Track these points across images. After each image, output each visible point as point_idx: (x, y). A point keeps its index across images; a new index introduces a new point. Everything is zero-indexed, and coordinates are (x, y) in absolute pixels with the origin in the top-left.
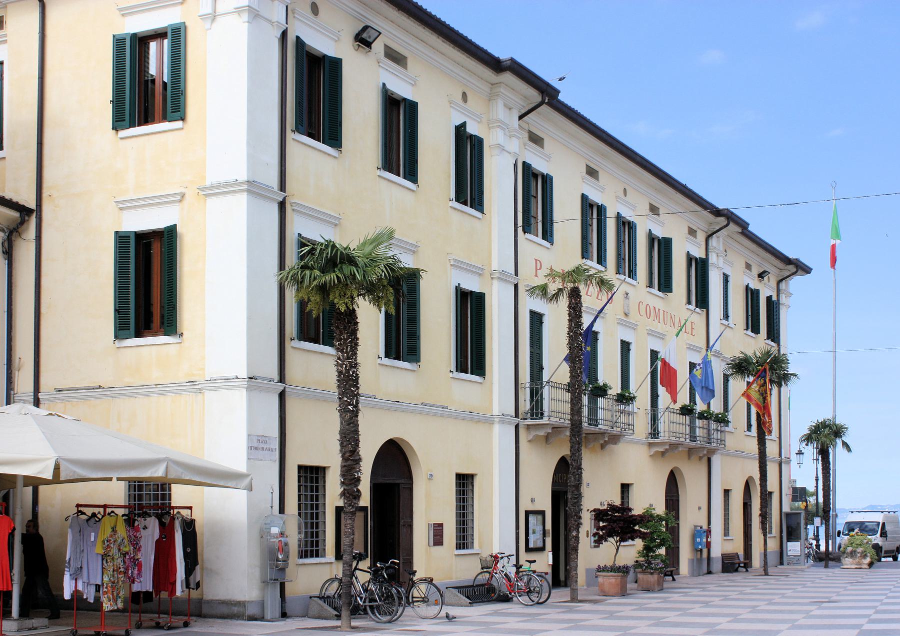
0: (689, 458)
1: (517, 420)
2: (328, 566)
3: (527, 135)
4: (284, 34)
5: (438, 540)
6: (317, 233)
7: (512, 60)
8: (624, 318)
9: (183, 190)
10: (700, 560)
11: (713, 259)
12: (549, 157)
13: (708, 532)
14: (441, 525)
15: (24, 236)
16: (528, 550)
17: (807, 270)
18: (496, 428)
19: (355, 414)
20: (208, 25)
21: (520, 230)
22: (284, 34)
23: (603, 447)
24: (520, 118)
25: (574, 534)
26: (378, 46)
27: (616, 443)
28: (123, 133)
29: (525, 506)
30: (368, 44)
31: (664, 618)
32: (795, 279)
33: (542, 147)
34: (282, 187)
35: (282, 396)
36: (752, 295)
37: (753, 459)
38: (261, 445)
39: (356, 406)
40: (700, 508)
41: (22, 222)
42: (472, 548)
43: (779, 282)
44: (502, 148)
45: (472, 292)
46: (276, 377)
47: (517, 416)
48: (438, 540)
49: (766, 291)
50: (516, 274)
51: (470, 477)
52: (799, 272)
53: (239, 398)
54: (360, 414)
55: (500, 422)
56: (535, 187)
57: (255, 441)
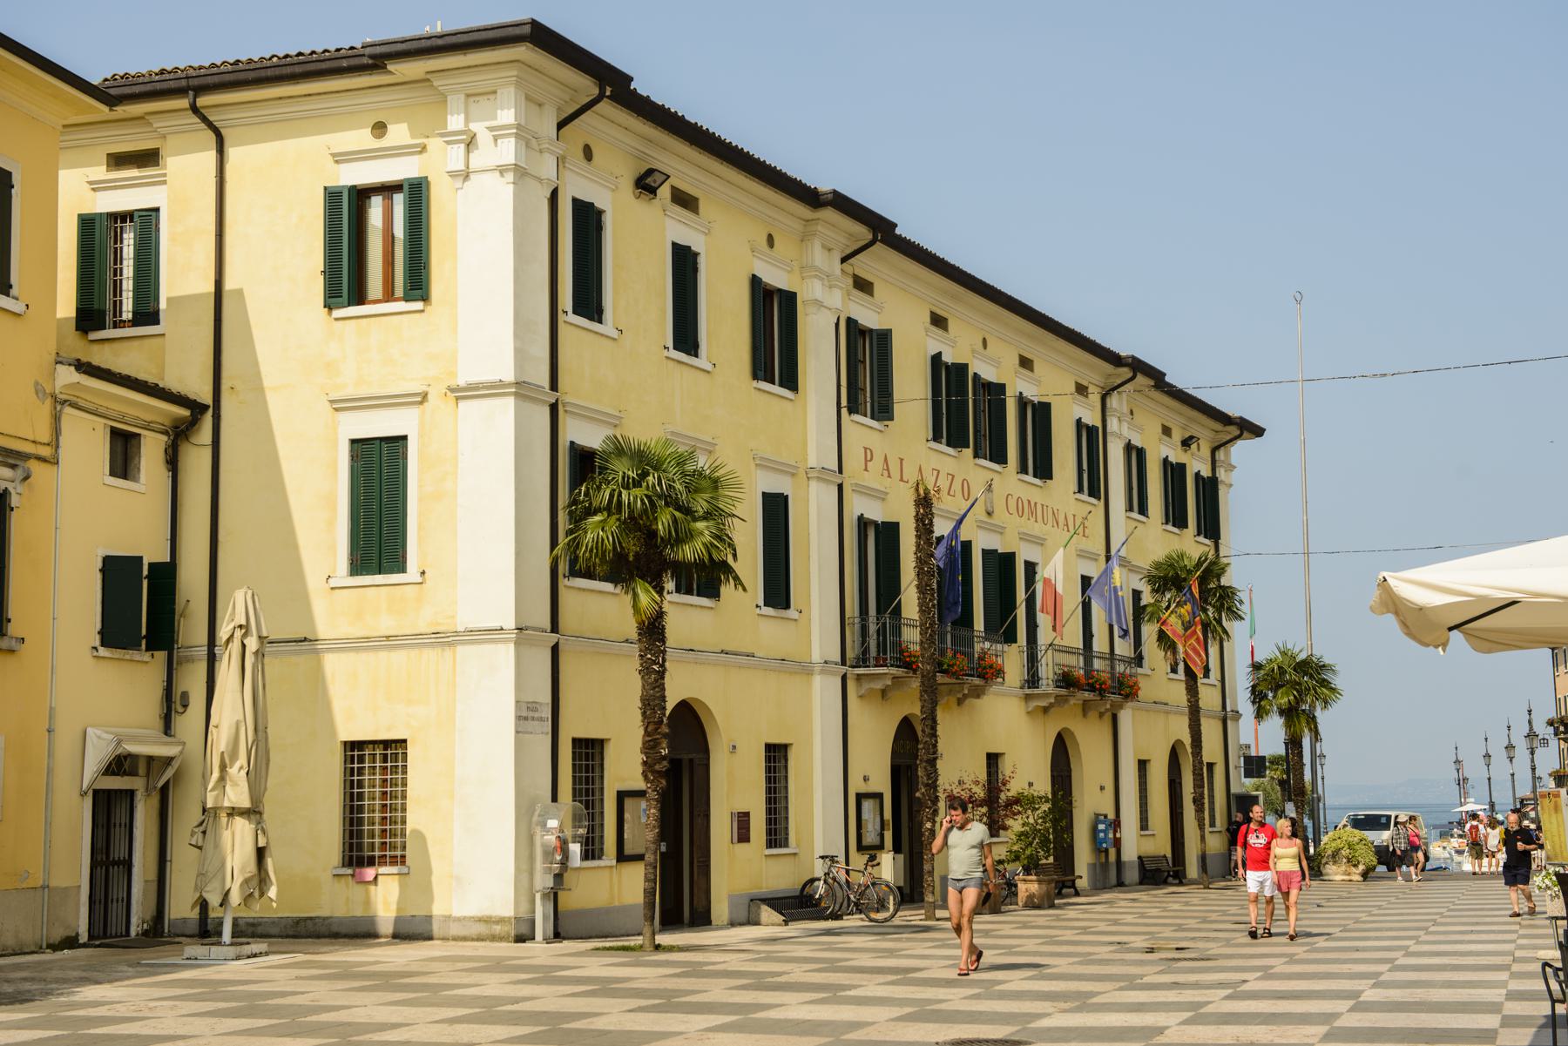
0: (1085, 715)
1: (843, 669)
2: (607, 872)
3: (850, 281)
4: (554, 195)
5: (743, 836)
6: (592, 438)
7: (835, 192)
8: (984, 518)
9: (425, 388)
10: (1105, 866)
11: (1113, 425)
12: (882, 308)
13: (1116, 824)
14: (747, 814)
15: (193, 440)
17: (1258, 432)
18: (817, 680)
19: (661, 674)
20: (459, 184)
21: (844, 411)
22: (554, 195)
23: (960, 702)
24: (844, 260)
25: (928, 825)
26: (664, 192)
27: (978, 697)
28: (337, 313)
29: (856, 786)
30: (652, 191)
32: (1240, 443)
33: (871, 294)
34: (554, 385)
35: (555, 650)
36: (1174, 473)
37: (1182, 714)
38: (531, 714)
39: (662, 666)
40: (1102, 788)
42: (786, 845)
43: (1214, 451)
44: (819, 304)
46: (548, 626)
47: (843, 663)
48: (743, 836)
49: (1197, 464)
50: (840, 471)
51: (784, 748)
52: (1246, 434)
53: (505, 654)
54: (667, 675)
55: (822, 672)
56: (867, 354)
57: (524, 707)
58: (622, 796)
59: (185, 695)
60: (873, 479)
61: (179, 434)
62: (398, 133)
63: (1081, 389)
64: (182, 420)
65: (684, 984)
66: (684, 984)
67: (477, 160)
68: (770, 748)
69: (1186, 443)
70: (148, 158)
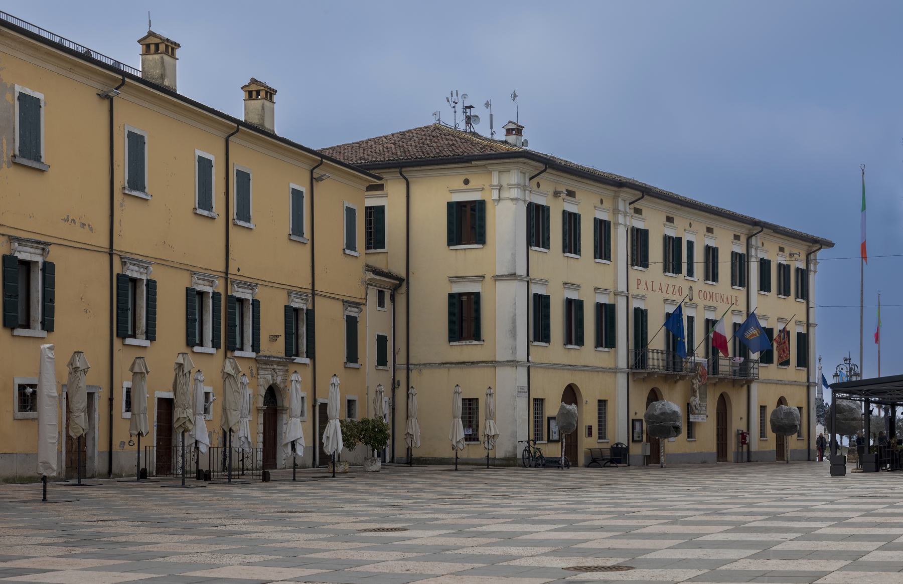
5: (590, 434)
16: (633, 441)
17: (830, 245)
29: (632, 416)
31: (726, 532)
41: (400, 285)
43: (808, 255)
45: (605, 304)
58: (549, 419)
59: (399, 381)
60: (641, 291)
61: (395, 289)
62: (474, 183)
63: (737, 237)
64: (396, 285)
65: (452, 541)
66: (452, 541)
67: (505, 194)
68: (599, 401)
69: (791, 255)
70: (381, 187)
